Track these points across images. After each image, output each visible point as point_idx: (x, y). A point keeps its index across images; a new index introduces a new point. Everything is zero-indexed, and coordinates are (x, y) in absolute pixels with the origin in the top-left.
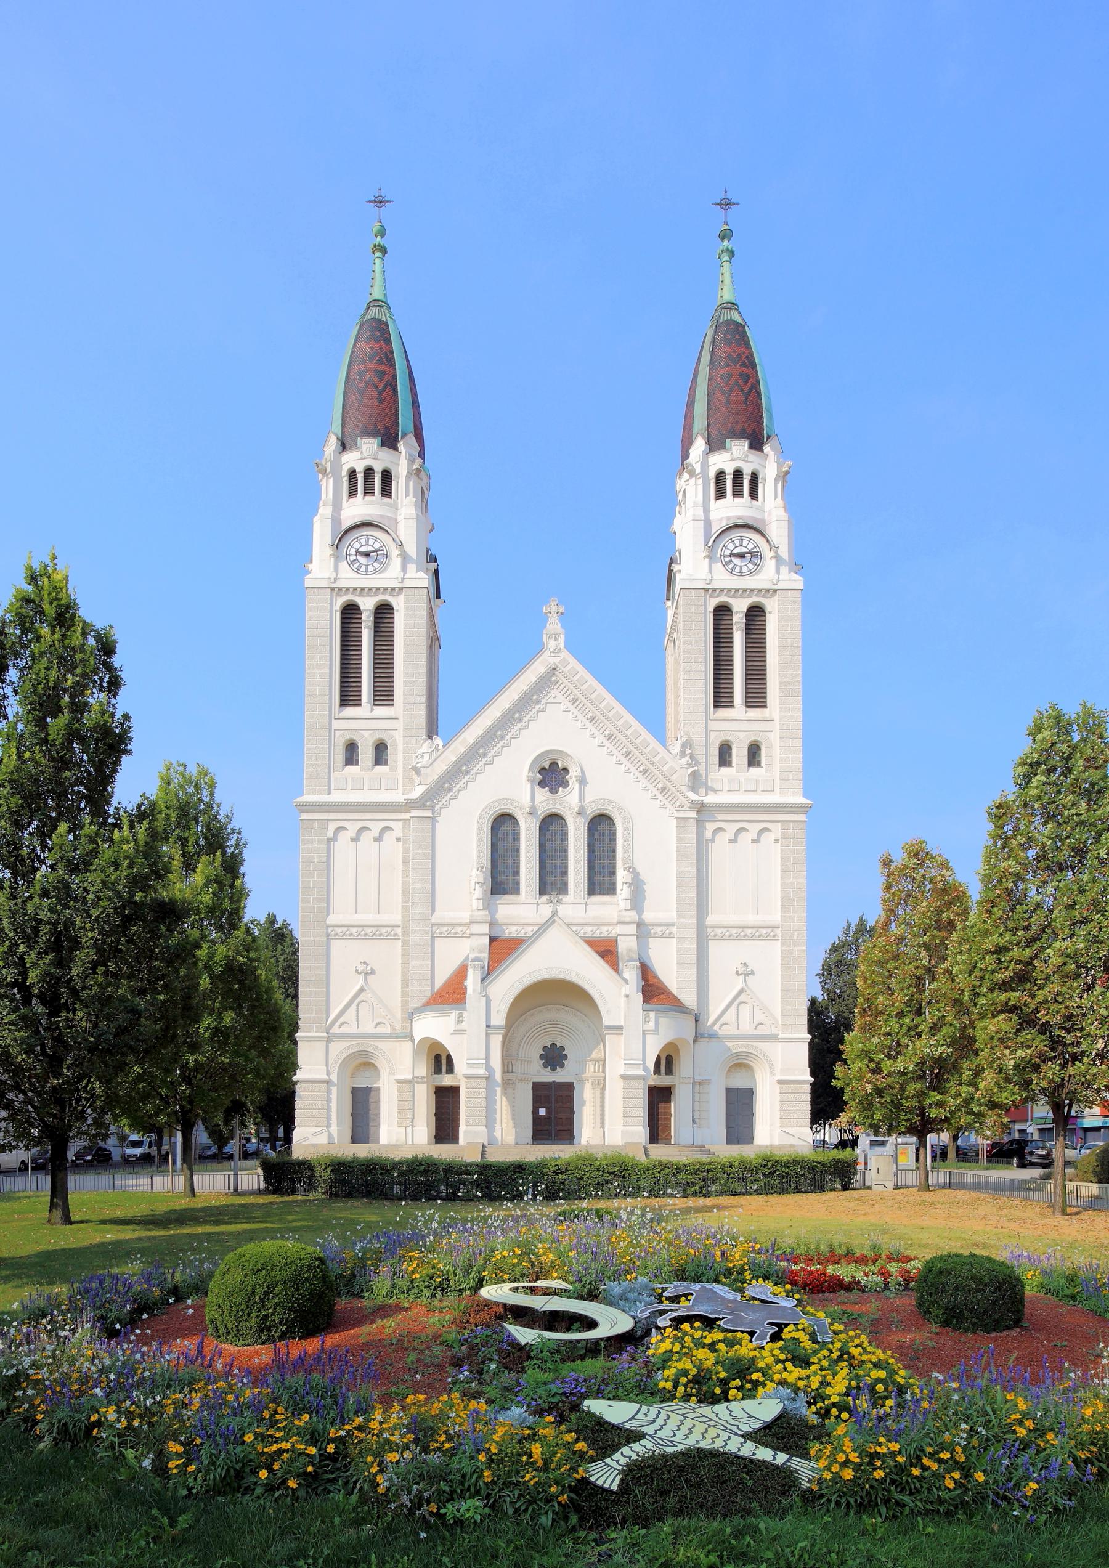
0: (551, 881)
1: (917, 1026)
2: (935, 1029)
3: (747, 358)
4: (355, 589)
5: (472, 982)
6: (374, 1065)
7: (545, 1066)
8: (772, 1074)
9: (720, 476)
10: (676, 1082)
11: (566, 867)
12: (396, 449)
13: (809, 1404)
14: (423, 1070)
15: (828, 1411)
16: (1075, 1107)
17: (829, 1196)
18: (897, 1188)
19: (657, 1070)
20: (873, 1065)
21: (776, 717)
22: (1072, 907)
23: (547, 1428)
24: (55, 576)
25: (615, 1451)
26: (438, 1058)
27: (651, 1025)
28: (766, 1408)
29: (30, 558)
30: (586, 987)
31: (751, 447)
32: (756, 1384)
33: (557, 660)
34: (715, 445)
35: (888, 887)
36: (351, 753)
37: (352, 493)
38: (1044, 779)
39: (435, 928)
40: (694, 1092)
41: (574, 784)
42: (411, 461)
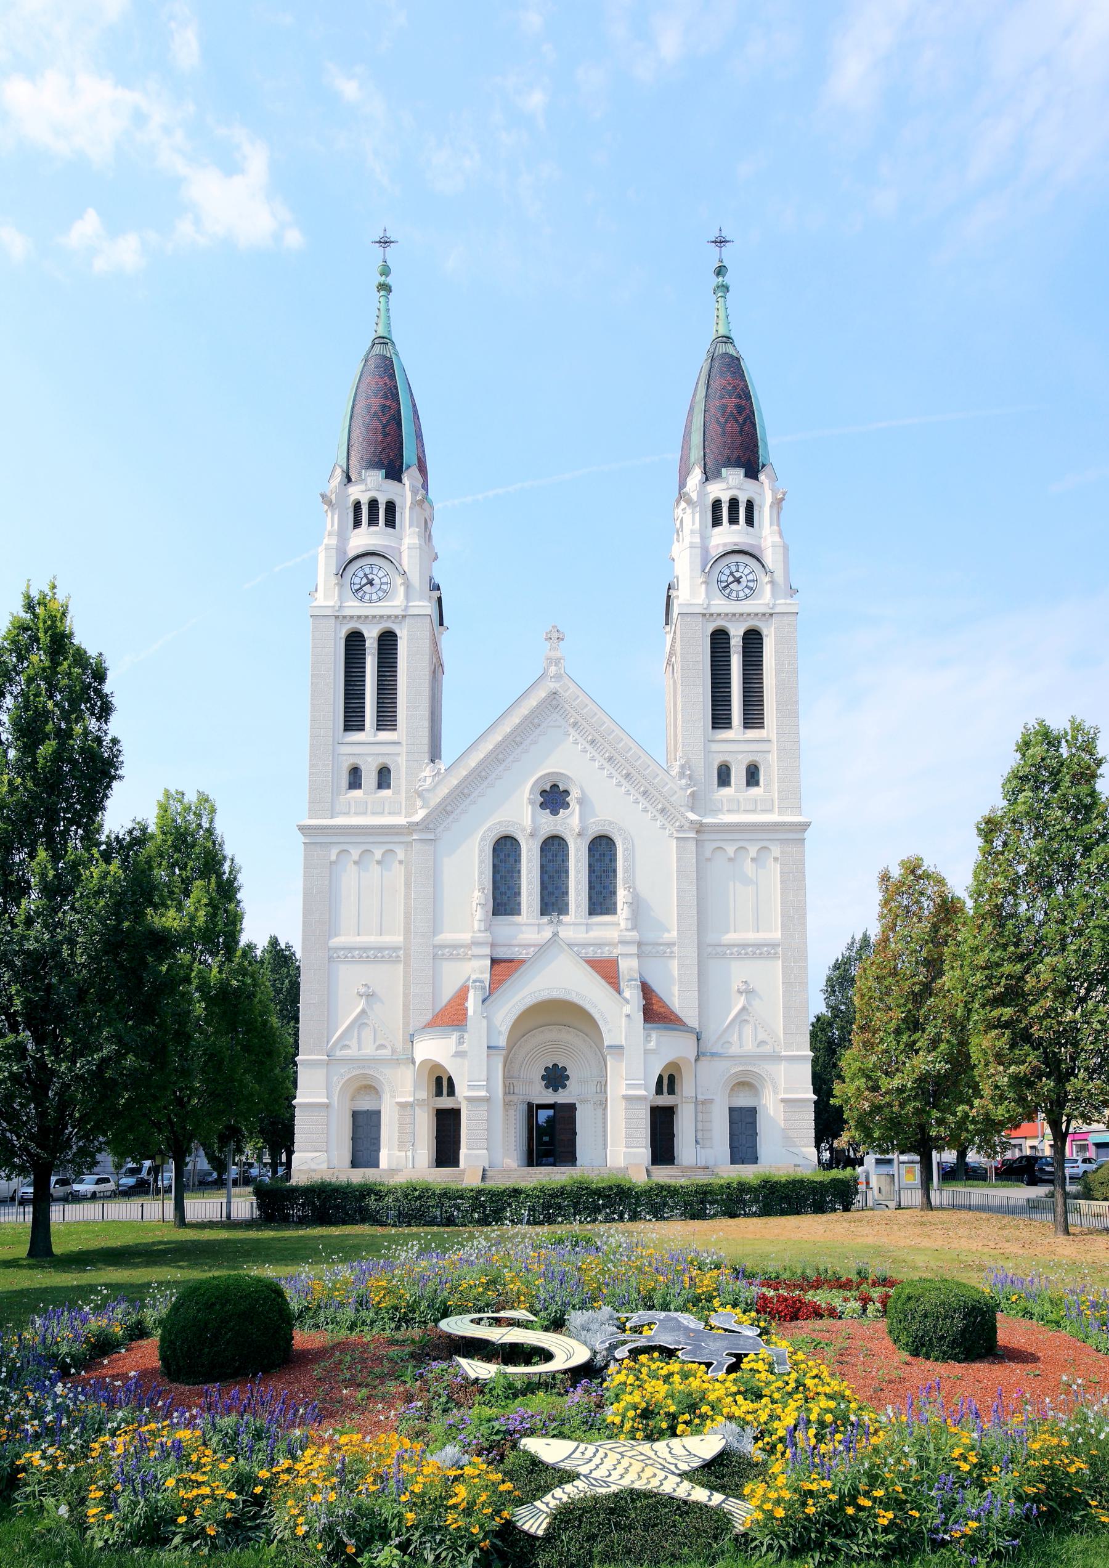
0: (553, 901)
1: (914, 1043)
2: (935, 1043)
3: (742, 389)
4: (359, 617)
6: (375, 1088)
7: (547, 1087)
8: (776, 1093)
9: (717, 505)
10: (679, 1102)
12: (400, 481)
13: (756, 1439)
14: (425, 1093)
15: (774, 1447)
16: (1073, 1123)
17: (832, 1216)
18: (899, 1207)
19: (659, 1090)
20: (870, 1084)
22: (1062, 922)
23: (476, 1466)
24: (51, 606)
25: (545, 1493)
26: (439, 1080)
28: (706, 1445)
29: (29, 586)
30: (588, 1007)
31: (747, 475)
32: (704, 1417)
33: (557, 685)
35: (886, 903)
36: (355, 778)
37: (357, 523)
38: (1031, 794)
39: (331, 952)
40: (696, 1112)
41: (574, 806)
42: (414, 492)
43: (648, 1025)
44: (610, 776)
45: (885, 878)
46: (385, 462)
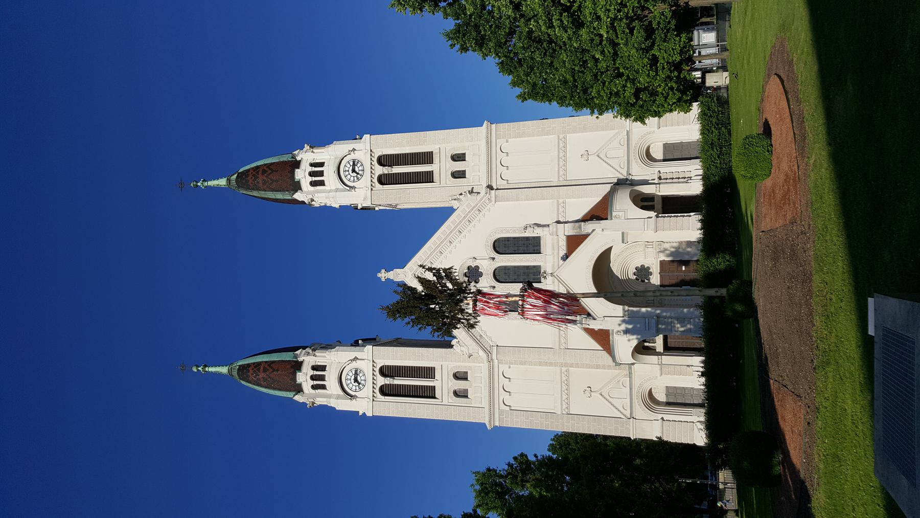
5: (595, 325)
8: (654, 132)
11: (524, 267)
12: (302, 362)
21: (438, 147)
27: (621, 214)
31: (298, 168)
33: (410, 273)
34: (297, 187)
45: (523, 97)
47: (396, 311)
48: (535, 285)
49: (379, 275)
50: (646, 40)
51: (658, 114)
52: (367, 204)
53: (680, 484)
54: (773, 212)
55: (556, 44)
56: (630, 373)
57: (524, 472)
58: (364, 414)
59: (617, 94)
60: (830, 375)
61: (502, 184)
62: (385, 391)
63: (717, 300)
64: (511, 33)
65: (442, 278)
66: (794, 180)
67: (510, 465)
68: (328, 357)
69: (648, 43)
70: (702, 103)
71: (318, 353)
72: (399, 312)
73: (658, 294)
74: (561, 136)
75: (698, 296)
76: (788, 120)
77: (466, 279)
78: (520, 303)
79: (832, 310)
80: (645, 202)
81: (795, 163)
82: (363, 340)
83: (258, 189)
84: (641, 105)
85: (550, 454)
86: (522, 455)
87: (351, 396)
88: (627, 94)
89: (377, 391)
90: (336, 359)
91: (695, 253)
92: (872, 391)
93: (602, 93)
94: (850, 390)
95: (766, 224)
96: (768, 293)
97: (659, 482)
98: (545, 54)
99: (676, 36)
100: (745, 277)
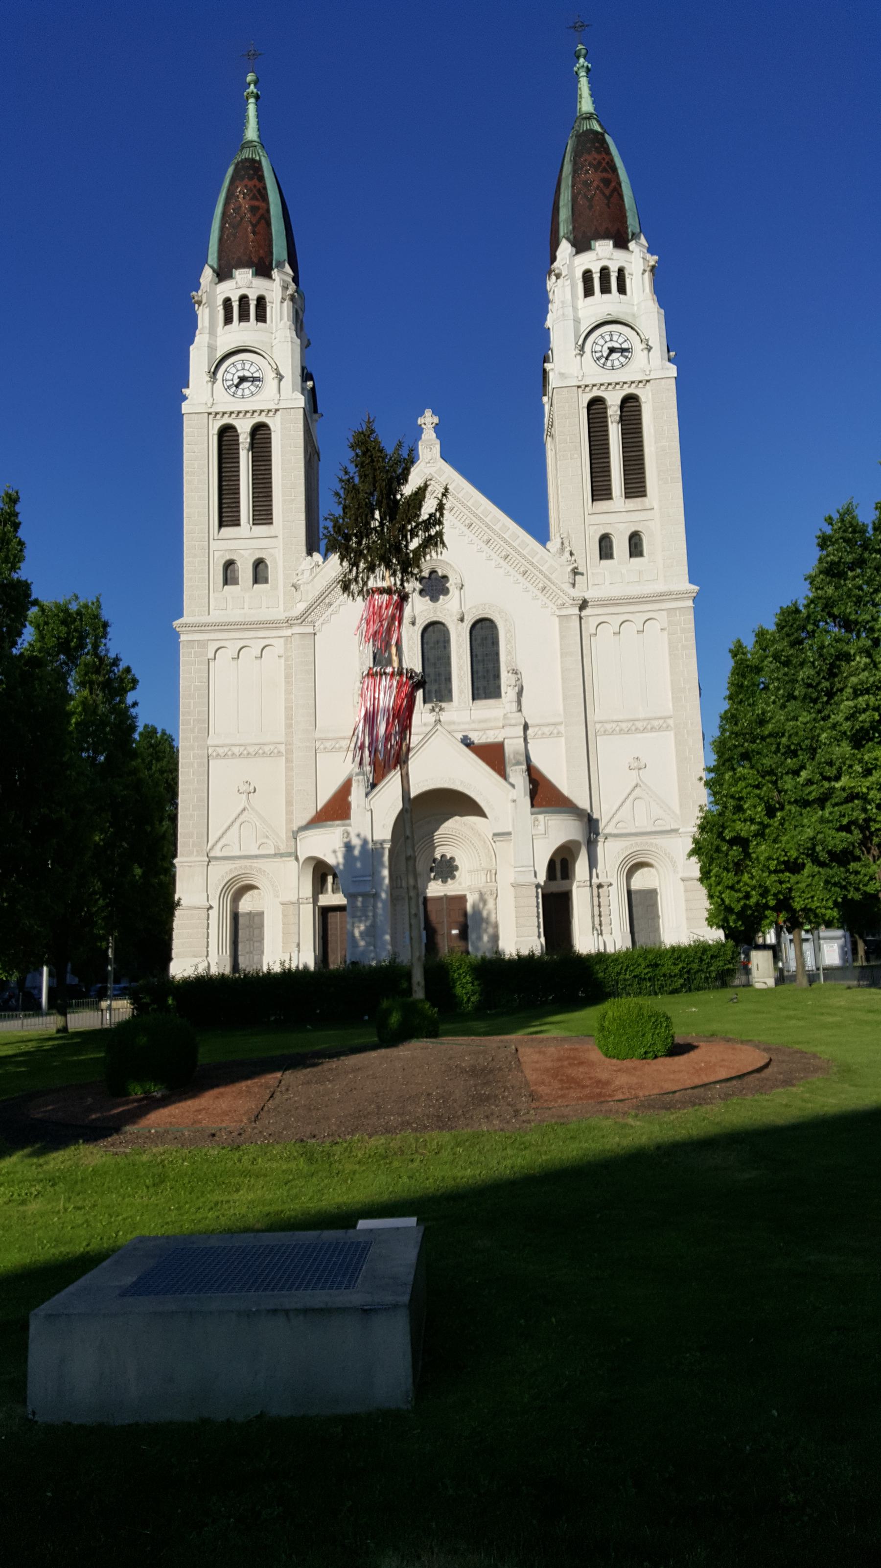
3: (608, 163)
5: (356, 797)
21: (655, 505)
27: (541, 828)
34: (581, 246)
37: (228, 320)
43: (536, 810)
44: (489, 559)
45: (737, 651)
46: (255, 260)
47: (366, 448)
48: (420, 694)
49: (428, 413)
50: (829, 852)
51: (705, 875)
52: (554, 380)
53: (104, 938)
54: (549, 1064)
55: (827, 702)
56: (282, 855)
57: (107, 685)
58: (185, 398)
59: (739, 809)
60: (293, 1165)
61: (590, 624)
62: (227, 434)
63: (405, 985)
64: (848, 625)
65: (427, 529)
66: (600, 1095)
67: (116, 662)
68: (281, 325)
69: (824, 856)
70: (723, 945)
71: (287, 305)
72: (364, 454)
73: (412, 894)
74: (671, 722)
75: (411, 956)
76: (697, 1081)
77: (425, 574)
78: (389, 670)
79: (396, 1164)
80: (561, 865)
81: (628, 1095)
82: (313, 389)
83: (575, 172)
84: (721, 848)
85: (140, 729)
86: (135, 682)
87: (215, 373)
88: (739, 826)
89: (226, 420)
90: (277, 340)
91: (479, 948)
92: (270, 1229)
93: (741, 784)
94: (269, 1196)
95: (529, 1055)
96: (417, 1061)
97: (107, 905)
98: (809, 686)
99: (836, 903)
100: (443, 1027)
